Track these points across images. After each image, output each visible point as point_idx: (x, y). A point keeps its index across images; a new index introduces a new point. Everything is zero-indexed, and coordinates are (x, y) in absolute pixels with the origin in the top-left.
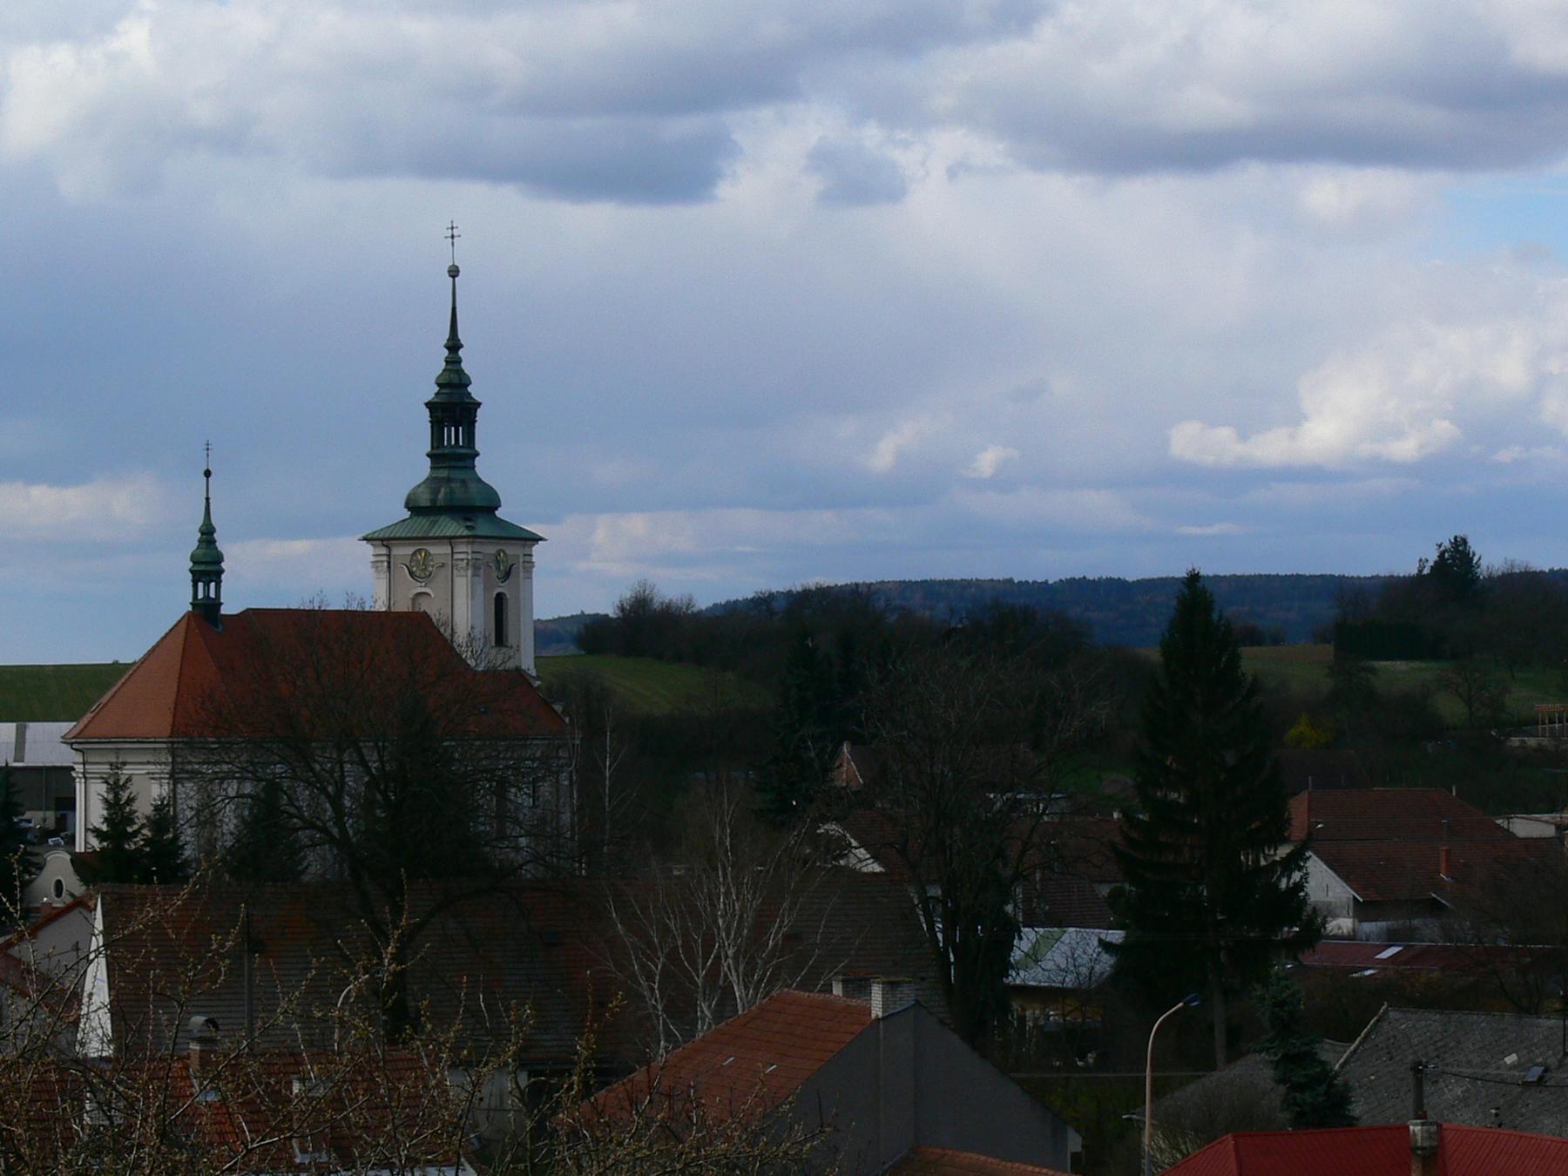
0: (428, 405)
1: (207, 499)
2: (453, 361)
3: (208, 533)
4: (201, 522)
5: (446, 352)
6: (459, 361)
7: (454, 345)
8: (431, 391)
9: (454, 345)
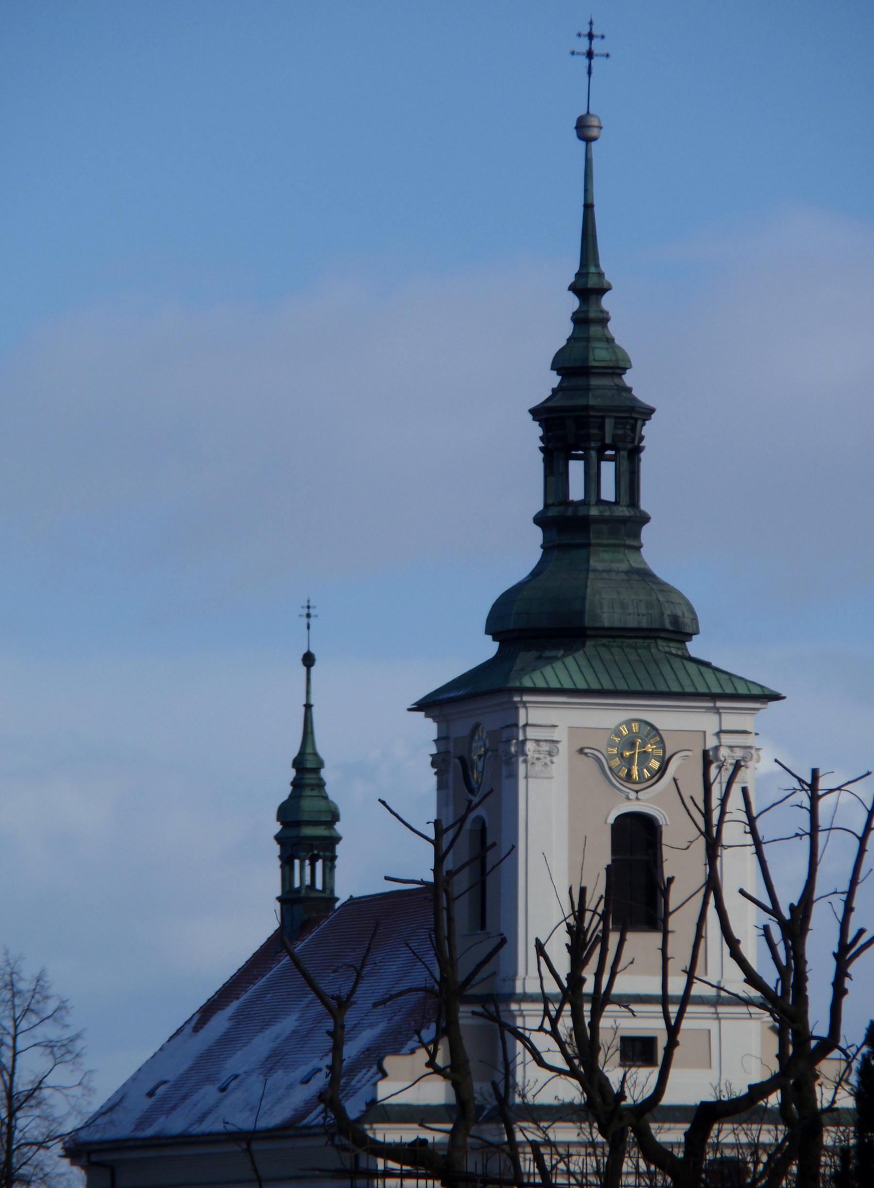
0: (537, 413)
1: (588, 208)
2: (588, 320)
3: (307, 769)
4: (294, 751)
5: (573, 303)
7: (588, 288)
9: (588, 288)
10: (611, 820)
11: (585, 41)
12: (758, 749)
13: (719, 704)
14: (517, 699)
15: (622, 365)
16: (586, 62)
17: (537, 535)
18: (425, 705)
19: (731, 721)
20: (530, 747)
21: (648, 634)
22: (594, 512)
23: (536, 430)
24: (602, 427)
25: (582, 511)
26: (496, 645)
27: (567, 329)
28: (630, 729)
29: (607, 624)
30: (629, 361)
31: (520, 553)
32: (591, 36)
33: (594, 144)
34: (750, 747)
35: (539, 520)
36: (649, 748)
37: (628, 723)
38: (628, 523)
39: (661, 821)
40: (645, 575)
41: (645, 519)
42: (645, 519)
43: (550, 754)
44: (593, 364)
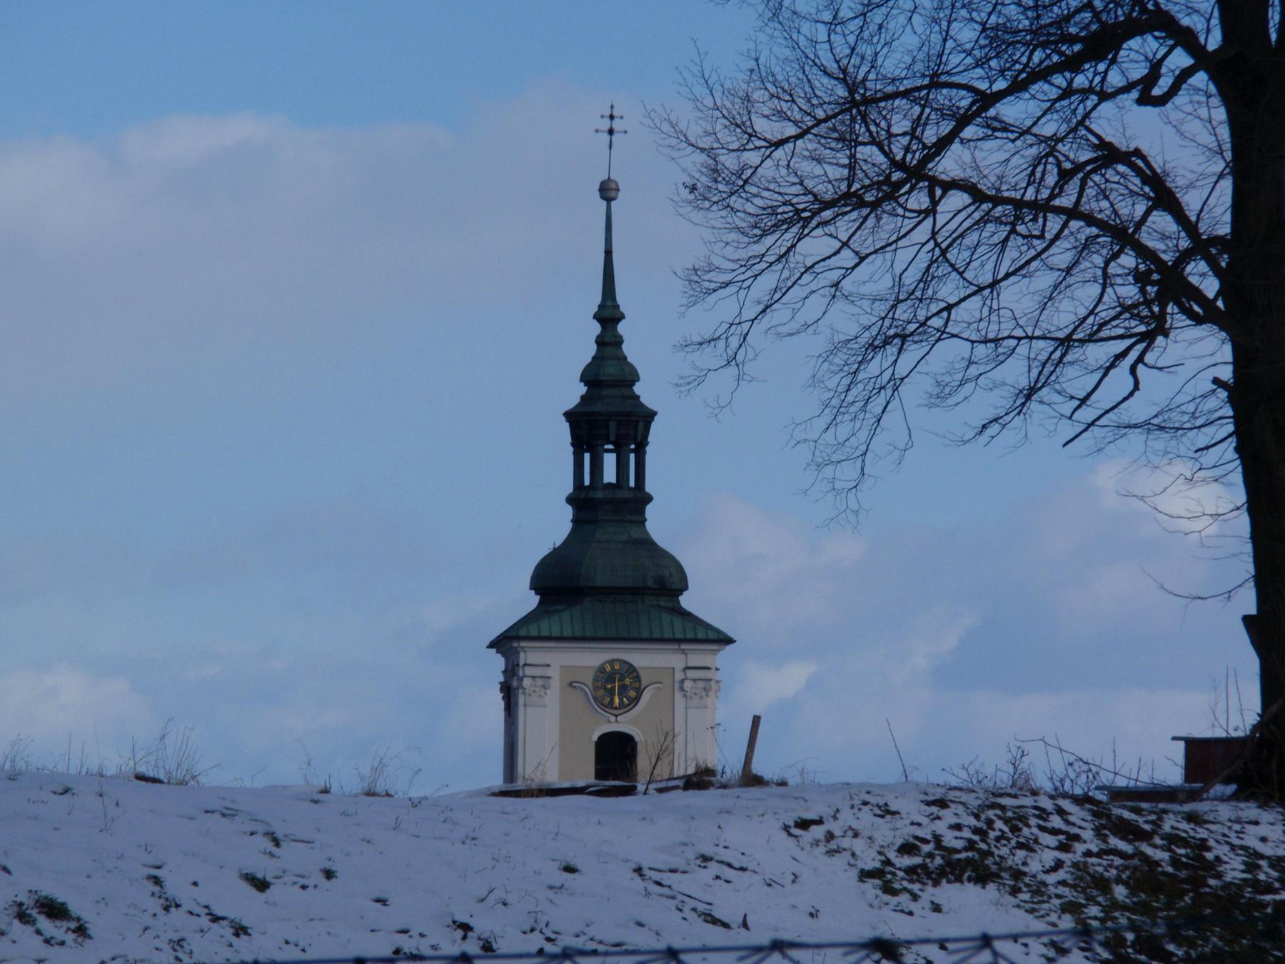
0: (569, 415)
1: (608, 253)
2: (609, 343)
5: (596, 328)
6: (618, 342)
7: (609, 316)
8: (574, 392)
9: (609, 316)
10: (595, 738)
11: (608, 120)
12: (718, 682)
13: (683, 646)
14: (515, 644)
15: (629, 378)
16: (608, 137)
17: (568, 512)
18: (491, 646)
19: (695, 660)
20: (527, 682)
21: (636, 592)
22: (599, 495)
23: (566, 427)
24: (607, 427)
25: (591, 494)
26: (538, 598)
27: (592, 349)
28: (612, 668)
29: (599, 585)
30: (637, 375)
31: (554, 525)
32: (612, 117)
33: (613, 203)
34: (710, 680)
35: (570, 500)
36: (627, 681)
37: (612, 662)
38: (633, 502)
39: (637, 739)
40: (649, 543)
41: (649, 499)
42: (649, 499)
43: (544, 687)
44: (603, 378)
